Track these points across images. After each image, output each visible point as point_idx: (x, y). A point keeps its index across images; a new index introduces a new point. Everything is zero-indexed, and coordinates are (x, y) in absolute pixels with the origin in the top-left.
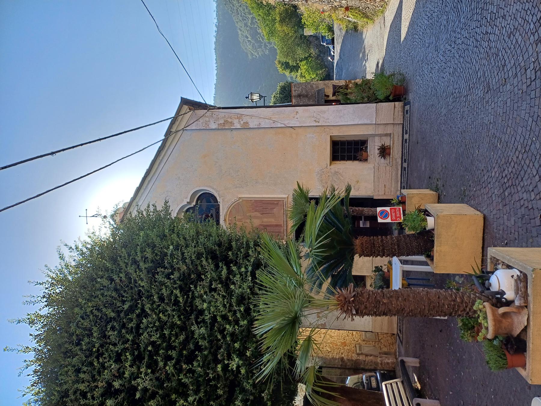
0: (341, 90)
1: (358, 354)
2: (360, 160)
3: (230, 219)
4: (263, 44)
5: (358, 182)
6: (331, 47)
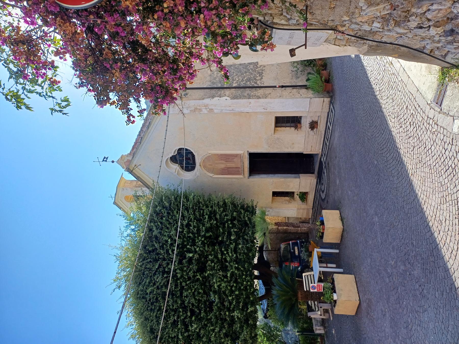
5: (293, 144)
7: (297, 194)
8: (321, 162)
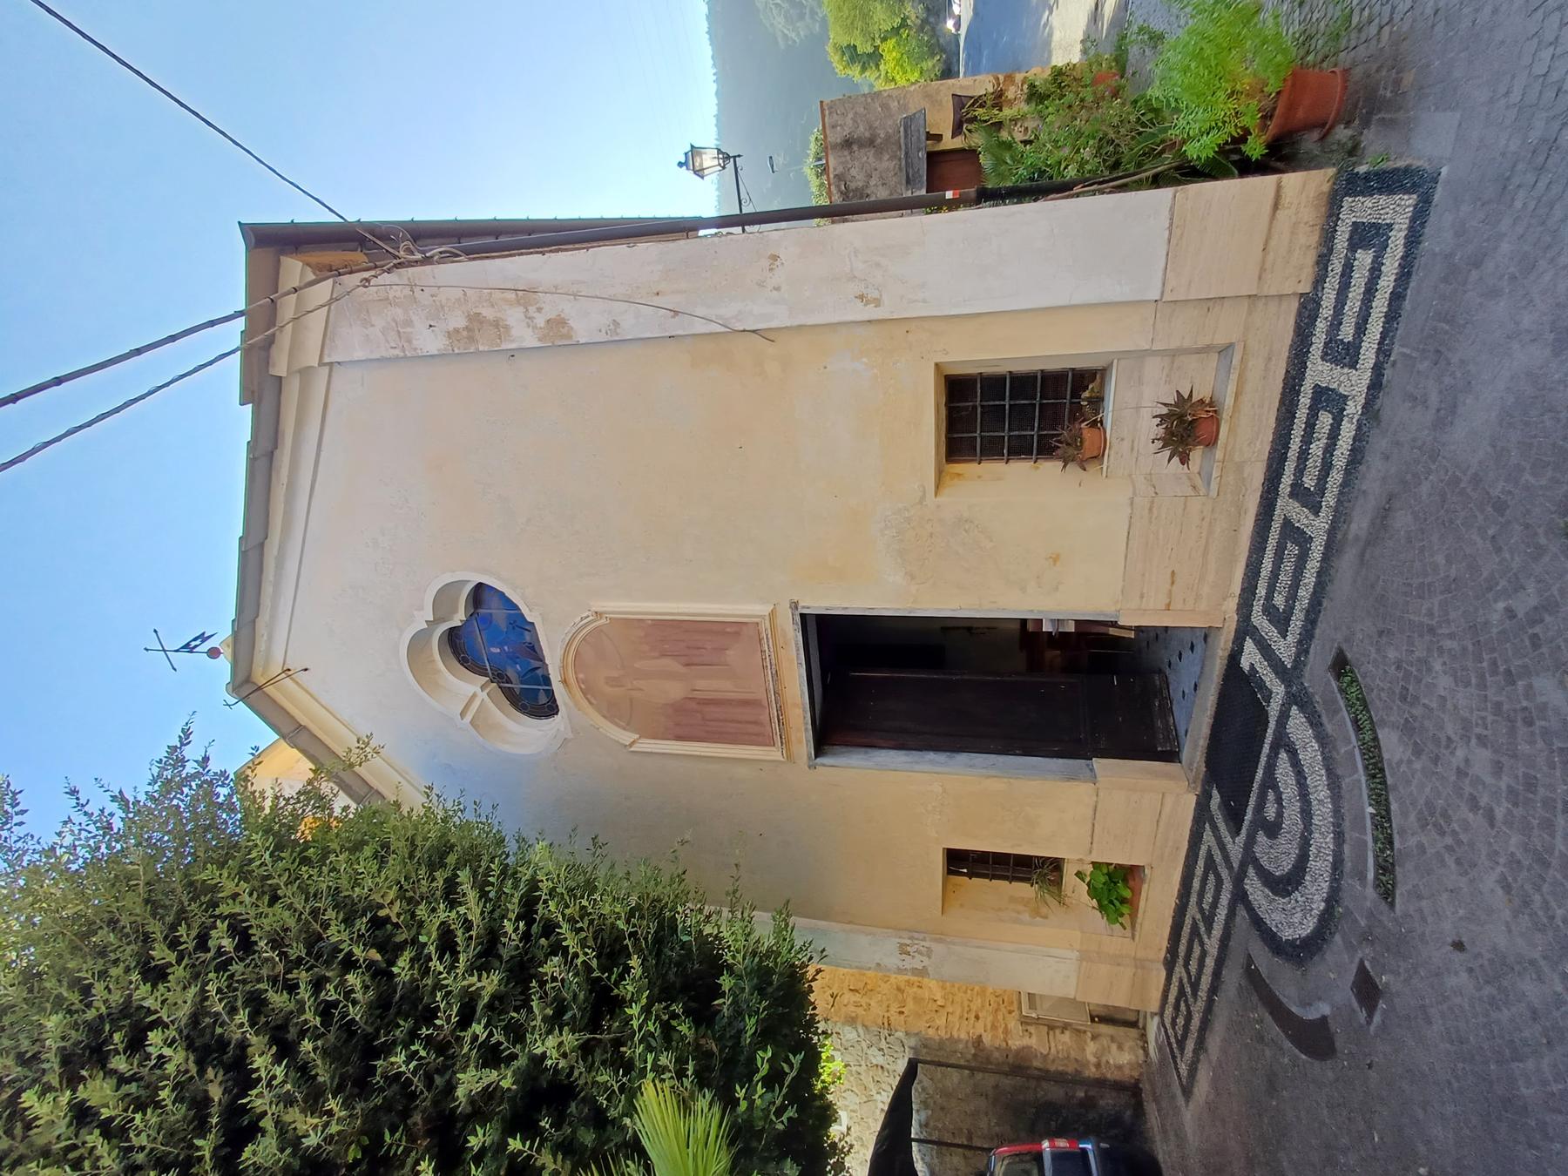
0: (981, 111)
1: (1025, 1021)
2: (1066, 461)
4: (807, 11)
5: (1055, 559)
7: (1079, 874)
8: (1238, 683)
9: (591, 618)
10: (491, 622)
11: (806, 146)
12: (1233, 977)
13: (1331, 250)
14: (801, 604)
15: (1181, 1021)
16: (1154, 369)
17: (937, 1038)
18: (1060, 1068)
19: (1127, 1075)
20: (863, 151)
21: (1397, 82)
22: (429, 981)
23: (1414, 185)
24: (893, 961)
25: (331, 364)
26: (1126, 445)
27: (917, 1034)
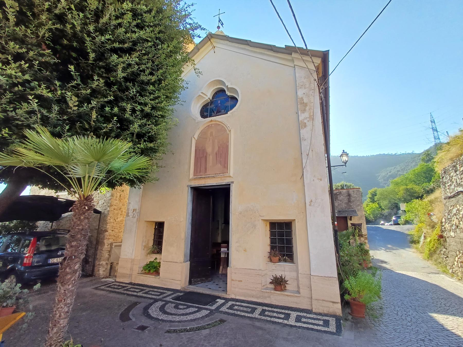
1: (111, 244)
2: (270, 253)
3: (213, 125)
4: (386, 182)
5: (245, 250)
6: (392, 223)
7: (156, 259)
8: (213, 299)
9: (229, 129)
10: (226, 101)
11: (349, 181)
12: (134, 299)
13: (323, 316)
14: (233, 184)
15: (116, 287)
16: (294, 274)
17: (107, 219)
18: (98, 254)
19: (96, 272)
20: (347, 199)
21: (361, 328)
22: (148, 94)
23: (338, 332)
24: (131, 207)
25: (295, 67)
26: (274, 268)
27: (108, 214)
